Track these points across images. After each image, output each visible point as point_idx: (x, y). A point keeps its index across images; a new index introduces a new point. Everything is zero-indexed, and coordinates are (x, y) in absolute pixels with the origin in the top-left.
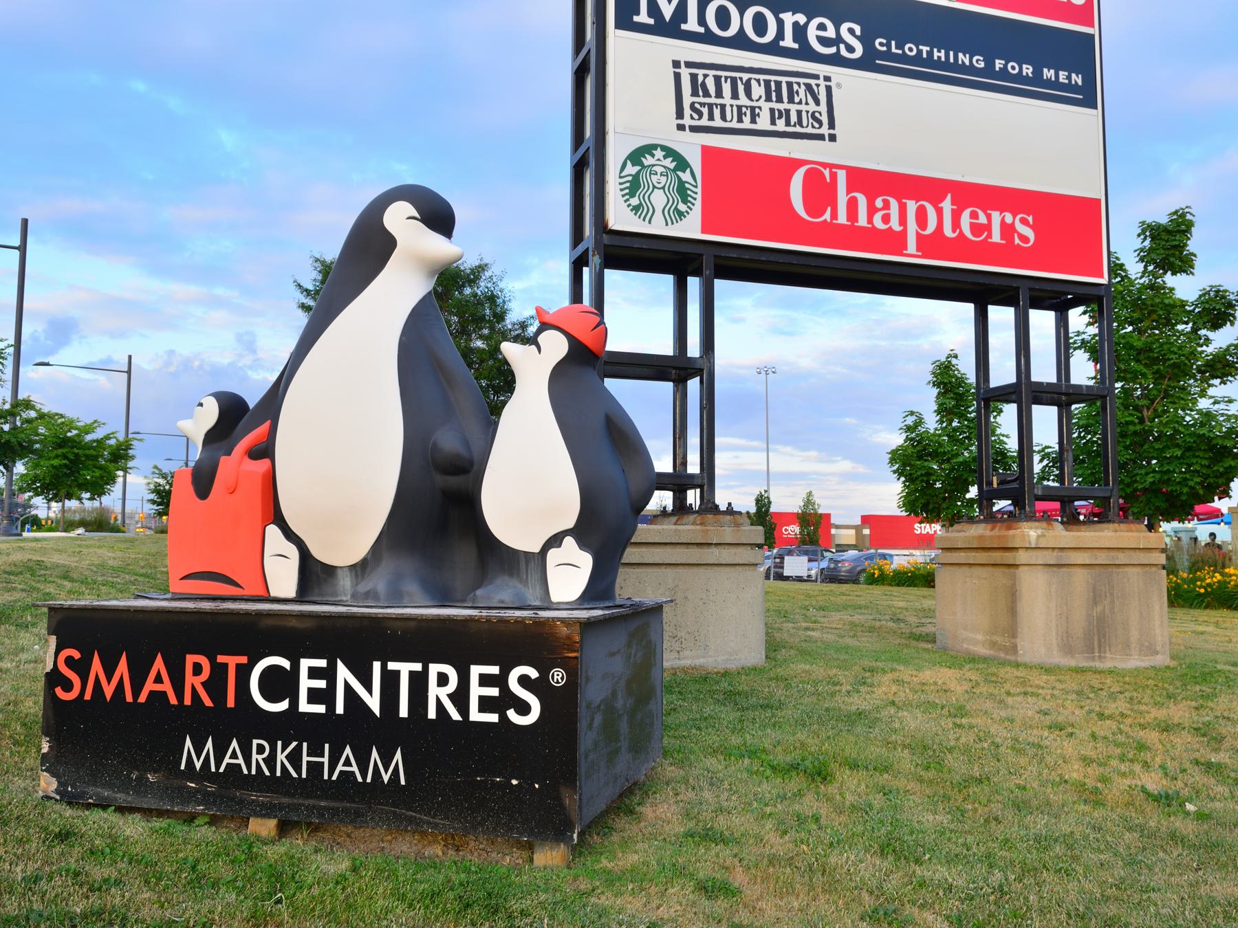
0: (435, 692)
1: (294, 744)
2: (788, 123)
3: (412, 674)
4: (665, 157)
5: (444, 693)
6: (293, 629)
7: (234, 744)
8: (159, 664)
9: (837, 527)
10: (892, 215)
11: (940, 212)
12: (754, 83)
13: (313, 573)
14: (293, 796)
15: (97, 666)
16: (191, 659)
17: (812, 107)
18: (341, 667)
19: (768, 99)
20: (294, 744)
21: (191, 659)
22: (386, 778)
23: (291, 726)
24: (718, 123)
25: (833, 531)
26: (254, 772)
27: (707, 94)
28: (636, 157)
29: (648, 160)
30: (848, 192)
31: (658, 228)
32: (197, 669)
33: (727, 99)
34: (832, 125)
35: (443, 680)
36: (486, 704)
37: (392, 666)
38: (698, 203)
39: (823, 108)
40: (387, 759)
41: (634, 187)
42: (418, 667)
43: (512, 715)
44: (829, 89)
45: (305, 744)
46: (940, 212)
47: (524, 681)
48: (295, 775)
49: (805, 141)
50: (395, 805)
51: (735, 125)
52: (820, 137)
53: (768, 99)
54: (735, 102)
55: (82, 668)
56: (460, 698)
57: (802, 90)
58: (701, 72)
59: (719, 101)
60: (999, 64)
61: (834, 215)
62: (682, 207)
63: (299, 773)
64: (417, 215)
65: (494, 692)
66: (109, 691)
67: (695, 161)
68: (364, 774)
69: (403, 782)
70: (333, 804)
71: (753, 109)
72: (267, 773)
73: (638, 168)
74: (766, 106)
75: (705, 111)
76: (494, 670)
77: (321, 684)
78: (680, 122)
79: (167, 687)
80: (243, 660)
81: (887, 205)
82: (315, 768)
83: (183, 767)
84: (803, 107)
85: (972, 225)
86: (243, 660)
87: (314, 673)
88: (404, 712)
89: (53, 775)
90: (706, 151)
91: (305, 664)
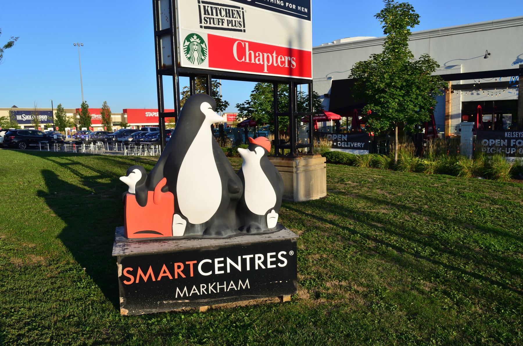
0: (257, 262)
2: (232, 26)
4: (197, 38)
5: (260, 262)
7: (194, 287)
8: (164, 267)
9: (114, 114)
11: (272, 57)
12: (222, 10)
13: (190, 227)
14: (215, 298)
15: (140, 272)
16: (176, 265)
17: (239, 19)
18: (228, 259)
19: (226, 16)
21: (176, 265)
22: (244, 287)
23: (214, 278)
24: (212, 25)
25: (112, 116)
27: (209, 14)
29: (192, 40)
30: (249, 50)
31: (196, 66)
32: (179, 267)
33: (215, 17)
34: (244, 27)
35: (259, 258)
36: (272, 263)
37: (244, 257)
38: (207, 56)
39: (242, 20)
41: (188, 50)
42: (252, 256)
43: (279, 265)
44: (243, 12)
46: (272, 57)
47: (283, 255)
48: (215, 292)
50: (247, 294)
51: (217, 26)
52: (241, 31)
53: (226, 16)
54: (217, 17)
55: (134, 273)
56: (265, 263)
57: (236, 13)
58: (206, 5)
59: (212, 17)
60: (287, 4)
61: (245, 60)
62: (203, 58)
65: (274, 259)
66: (145, 279)
67: (206, 40)
68: (237, 288)
71: (222, 20)
74: (226, 19)
75: (208, 20)
76: (274, 254)
77: (222, 265)
78: (201, 25)
79: (168, 274)
80: (196, 262)
81: (259, 56)
82: (222, 289)
84: (236, 19)
85: (281, 61)
86: (196, 262)
87: (219, 262)
88: (248, 269)
89: (126, 308)
90: (209, 36)
91: (216, 260)
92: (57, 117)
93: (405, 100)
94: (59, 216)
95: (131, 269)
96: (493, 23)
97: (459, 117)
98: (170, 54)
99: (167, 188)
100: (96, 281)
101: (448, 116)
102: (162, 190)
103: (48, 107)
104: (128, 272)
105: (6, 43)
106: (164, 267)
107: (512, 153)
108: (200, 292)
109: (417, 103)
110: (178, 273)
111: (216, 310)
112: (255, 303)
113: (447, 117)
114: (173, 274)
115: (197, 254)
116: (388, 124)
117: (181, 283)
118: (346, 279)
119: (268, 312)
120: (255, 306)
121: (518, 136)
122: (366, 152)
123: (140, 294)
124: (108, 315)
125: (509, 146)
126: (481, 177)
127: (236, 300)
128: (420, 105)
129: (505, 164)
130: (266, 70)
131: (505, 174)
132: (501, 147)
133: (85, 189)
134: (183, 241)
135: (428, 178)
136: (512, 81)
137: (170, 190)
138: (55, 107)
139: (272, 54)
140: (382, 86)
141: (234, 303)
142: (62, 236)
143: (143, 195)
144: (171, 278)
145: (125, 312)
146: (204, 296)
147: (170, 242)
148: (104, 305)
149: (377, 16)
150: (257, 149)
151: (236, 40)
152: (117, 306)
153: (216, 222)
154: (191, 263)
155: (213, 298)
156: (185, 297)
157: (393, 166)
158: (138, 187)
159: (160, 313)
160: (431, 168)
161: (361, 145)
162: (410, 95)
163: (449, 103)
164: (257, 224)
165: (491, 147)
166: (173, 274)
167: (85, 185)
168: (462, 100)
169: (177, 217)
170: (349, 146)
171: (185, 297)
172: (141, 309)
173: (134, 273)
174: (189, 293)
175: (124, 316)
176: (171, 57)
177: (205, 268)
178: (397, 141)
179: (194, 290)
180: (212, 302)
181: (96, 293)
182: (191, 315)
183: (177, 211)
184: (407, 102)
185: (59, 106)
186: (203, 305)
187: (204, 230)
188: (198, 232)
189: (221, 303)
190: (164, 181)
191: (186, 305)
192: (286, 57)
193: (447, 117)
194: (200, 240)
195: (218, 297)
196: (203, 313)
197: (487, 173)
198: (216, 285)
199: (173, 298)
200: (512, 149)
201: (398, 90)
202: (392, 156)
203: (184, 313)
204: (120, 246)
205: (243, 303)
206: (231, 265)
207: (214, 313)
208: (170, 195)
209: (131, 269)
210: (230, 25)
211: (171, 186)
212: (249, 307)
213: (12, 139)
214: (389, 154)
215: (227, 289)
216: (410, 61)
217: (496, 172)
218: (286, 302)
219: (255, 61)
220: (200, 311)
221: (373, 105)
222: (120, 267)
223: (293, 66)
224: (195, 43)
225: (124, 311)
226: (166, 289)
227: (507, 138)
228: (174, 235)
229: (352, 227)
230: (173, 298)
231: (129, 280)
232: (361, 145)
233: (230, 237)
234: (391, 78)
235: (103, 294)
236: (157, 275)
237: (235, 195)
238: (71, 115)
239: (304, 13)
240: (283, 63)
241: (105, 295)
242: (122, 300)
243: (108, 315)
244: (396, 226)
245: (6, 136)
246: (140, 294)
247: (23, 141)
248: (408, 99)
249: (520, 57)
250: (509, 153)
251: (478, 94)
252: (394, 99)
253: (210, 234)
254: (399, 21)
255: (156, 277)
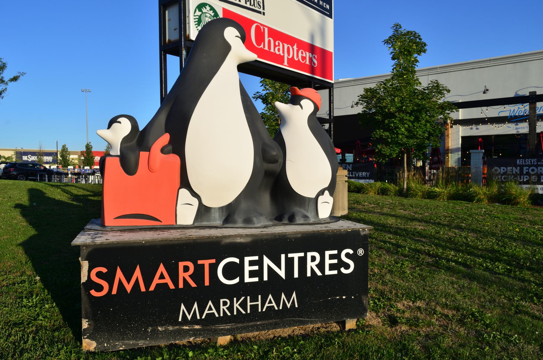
0: (310, 265)
1: (243, 298)
2: (250, 5)
3: (300, 258)
4: (210, 10)
5: (314, 265)
6: (241, 244)
7: (210, 303)
8: (162, 269)
10: (280, 49)
11: (293, 49)
13: (203, 211)
14: (243, 322)
15: (119, 275)
16: (181, 265)
18: (265, 258)
20: (243, 298)
21: (181, 265)
26: (222, 315)
28: (201, 7)
29: (204, 10)
30: (268, 37)
32: (186, 269)
34: (264, 9)
36: (332, 267)
37: (290, 255)
40: (289, 297)
42: (302, 254)
43: (343, 270)
45: (248, 297)
46: (293, 49)
47: (347, 255)
48: (244, 312)
49: (256, 13)
50: (293, 317)
52: (260, 12)
56: (321, 266)
61: (264, 46)
63: (246, 311)
64: (240, 36)
65: (335, 261)
66: (129, 287)
68: (278, 306)
69: (297, 306)
70: (264, 322)
72: (229, 314)
73: (201, 13)
76: (335, 252)
77: (256, 268)
79: (168, 280)
80: (213, 261)
81: (279, 45)
83: (180, 320)
86: (213, 261)
87: (251, 263)
88: (296, 275)
91: (247, 259)
92: (61, 156)
93: (414, 126)
94: (30, 224)
95: (104, 270)
96: (490, 60)
97: (458, 151)
98: (178, 27)
99: (170, 147)
100: (54, 298)
101: (448, 150)
102: (163, 151)
103: (53, 149)
104: (99, 275)
105: (12, 77)
106: (162, 269)
107: (525, 180)
108: (219, 313)
109: (426, 130)
110: (184, 278)
111: (243, 341)
112: (302, 332)
113: (447, 151)
114: (175, 280)
115: (216, 249)
116: (397, 150)
117: (188, 296)
118: (420, 298)
119: (328, 346)
120: (305, 337)
121: (531, 163)
122: (372, 181)
123: (118, 313)
124: (59, 350)
125: (521, 173)
126: (498, 203)
127: (275, 326)
128: (429, 132)
129: (522, 191)
130: (286, 63)
131: (524, 199)
132: (513, 174)
133: (72, 204)
134: (194, 230)
135: (441, 203)
136: (511, 116)
137: (174, 152)
138: (60, 149)
139: (292, 46)
140: (393, 109)
141: (270, 332)
142: (28, 246)
143: (132, 157)
144: (172, 286)
145: (89, 345)
146: (225, 319)
147: (172, 231)
148: (56, 334)
149: (385, 43)
150: (303, 102)
151: (255, 22)
152: (78, 335)
153: (244, 205)
154: (206, 263)
155: (239, 323)
156: (194, 320)
157: (401, 193)
158: (125, 145)
159: (152, 348)
160: (444, 195)
161: (366, 175)
162: (420, 121)
163: (448, 137)
164: (302, 211)
165: (502, 175)
166: (175, 280)
167: (73, 201)
168: (461, 134)
169: (184, 193)
170: (354, 176)
171: (194, 320)
172: (118, 340)
173: (109, 277)
174: (201, 314)
175: (89, 352)
176: (178, 31)
177: (229, 271)
178: (406, 169)
179: (210, 309)
180: (238, 328)
181: (50, 313)
182: (205, 350)
183: (185, 183)
184: (417, 128)
185: (64, 147)
186: (224, 335)
187: (224, 218)
188: (215, 220)
189: (252, 331)
190: (165, 139)
191: (196, 333)
192: (307, 53)
193: (447, 151)
194: (219, 229)
195: (248, 321)
196: (225, 347)
197: (504, 199)
198: (245, 301)
199: (175, 322)
200: (525, 176)
201: (408, 115)
202: (400, 185)
203: (193, 347)
204: (89, 234)
205: (286, 332)
206: (269, 268)
207: (242, 347)
208: (176, 159)
209: (104, 270)
210: (248, 3)
211: (177, 146)
212: (296, 338)
213: (11, 172)
214: (396, 182)
215: (262, 308)
216: (418, 88)
217: (515, 198)
218: (350, 330)
219: (274, 50)
220: (218, 344)
221: (382, 131)
222: (85, 265)
223: (315, 64)
224: (207, 14)
225: (89, 345)
226: (163, 305)
227: (519, 166)
228: (178, 223)
229: (393, 241)
230: (175, 322)
231: (99, 288)
232: (366, 175)
233: (265, 227)
234: (402, 102)
235: (60, 317)
236: (148, 279)
237: (272, 166)
238: (76, 156)
239: (326, 9)
240: (304, 58)
241: (64, 319)
242: (85, 324)
243: (59, 350)
244: (444, 241)
245: (5, 168)
246: (118, 313)
247: (20, 170)
248: (418, 125)
249: (518, 93)
250: (522, 180)
251: (477, 129)
252: (404, 124)
253: (234, 222)
254: (406, 46)
255: (148, 284)
